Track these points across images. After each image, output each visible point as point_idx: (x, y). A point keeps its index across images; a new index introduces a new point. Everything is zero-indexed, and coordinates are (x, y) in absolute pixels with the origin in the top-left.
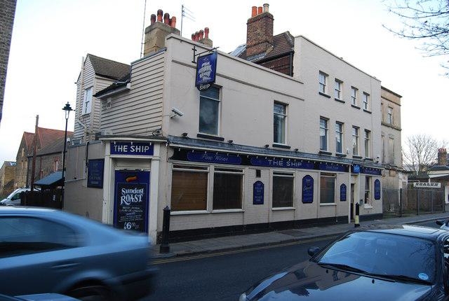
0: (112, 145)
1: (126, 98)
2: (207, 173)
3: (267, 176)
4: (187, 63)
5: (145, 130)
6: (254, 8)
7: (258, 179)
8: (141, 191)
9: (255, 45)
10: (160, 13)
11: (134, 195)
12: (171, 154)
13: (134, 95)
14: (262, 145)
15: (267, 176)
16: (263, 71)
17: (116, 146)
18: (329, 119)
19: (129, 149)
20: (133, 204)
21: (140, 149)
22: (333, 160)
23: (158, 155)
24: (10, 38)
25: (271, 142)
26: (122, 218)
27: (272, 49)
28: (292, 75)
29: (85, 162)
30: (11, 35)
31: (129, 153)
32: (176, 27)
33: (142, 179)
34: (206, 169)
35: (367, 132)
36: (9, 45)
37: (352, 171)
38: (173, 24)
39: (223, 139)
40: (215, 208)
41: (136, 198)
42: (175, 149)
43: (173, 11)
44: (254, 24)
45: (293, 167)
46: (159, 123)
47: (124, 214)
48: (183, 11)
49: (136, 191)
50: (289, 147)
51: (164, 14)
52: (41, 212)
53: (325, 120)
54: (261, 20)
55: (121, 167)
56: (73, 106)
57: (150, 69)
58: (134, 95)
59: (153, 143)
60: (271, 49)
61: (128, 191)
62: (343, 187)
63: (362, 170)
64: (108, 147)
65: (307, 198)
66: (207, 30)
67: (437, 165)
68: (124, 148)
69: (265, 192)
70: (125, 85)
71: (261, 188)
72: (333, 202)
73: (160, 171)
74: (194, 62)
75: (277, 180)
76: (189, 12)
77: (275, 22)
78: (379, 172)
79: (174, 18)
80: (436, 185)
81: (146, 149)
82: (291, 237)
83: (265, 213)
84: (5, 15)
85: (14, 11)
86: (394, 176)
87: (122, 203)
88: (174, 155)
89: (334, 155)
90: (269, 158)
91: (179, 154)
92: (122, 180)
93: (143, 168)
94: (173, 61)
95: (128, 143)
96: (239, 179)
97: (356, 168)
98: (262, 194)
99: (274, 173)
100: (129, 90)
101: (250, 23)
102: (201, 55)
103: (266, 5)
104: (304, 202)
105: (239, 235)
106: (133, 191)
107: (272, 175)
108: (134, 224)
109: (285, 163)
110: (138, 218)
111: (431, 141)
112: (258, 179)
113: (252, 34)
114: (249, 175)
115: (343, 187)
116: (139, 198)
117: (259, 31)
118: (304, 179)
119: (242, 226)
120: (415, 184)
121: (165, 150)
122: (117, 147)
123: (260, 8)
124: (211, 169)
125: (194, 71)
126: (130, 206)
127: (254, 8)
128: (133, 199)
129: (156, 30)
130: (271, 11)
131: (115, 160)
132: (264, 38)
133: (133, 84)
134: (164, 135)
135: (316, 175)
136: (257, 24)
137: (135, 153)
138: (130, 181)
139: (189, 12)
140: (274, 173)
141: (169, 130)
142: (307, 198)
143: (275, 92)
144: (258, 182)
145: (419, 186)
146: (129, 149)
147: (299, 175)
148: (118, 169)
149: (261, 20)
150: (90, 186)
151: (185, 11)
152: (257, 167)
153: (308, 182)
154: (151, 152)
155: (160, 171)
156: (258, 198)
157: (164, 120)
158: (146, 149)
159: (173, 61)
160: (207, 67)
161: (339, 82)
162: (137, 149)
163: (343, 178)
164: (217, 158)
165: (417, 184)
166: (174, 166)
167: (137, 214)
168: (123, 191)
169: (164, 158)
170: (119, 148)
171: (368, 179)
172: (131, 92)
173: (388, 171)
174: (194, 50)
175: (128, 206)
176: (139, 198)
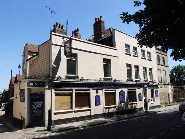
3: (102, 93)
7: (97, 94)
8: (41, 102)
10: (57, 24)
11: (38, 104)
14: (99, 79)
15: (102, 93)
20: (38, 108)
22: (134, 82)
25: (102, 76)
48: (67, 22)
51: (59, 24)
53: (129, 66)
56: (21, 66)
59: (45, 82)
63: (149, 86)
66: (78, 30)
69: (101, 99)
71: (99, 98)
75: (129, 92)
77: (105, 24)
78: (157, 86)
86: (167, 87)
89: (134, 80)
96: (88, 95)
98: (100, 100)
102: (66, 41)
104: (96, 105)
106: (37, 103)
109: (110, 85)
112: (97, 94)
114: (93, 93)
115: (140, 94)
116: (40, 106)
118: (120, 92)
122: (30, 84)
123: (98, 18)
126: (36, 109)
128: (38, 106)
135: (126, 91)
138: (36, 98)
153: (122, 94)
156: (98, 103)
160: (68, 45)
162: (38, 84)
167: (40, 113)
170: (30, 84)
173: (164, 85)
174: (63, 39)
176: (40, 106)
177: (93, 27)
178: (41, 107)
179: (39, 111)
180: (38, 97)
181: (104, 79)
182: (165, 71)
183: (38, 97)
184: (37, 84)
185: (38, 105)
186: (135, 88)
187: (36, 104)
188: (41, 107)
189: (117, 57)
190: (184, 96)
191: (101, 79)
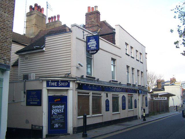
0: (48, 82)
1: (42, 55)
2: (89, 96)
3: (110, 95)
4: (80, 39)
5: (58, 73)
6: (89, 8)
8: (63, 106)
9: (91, 27)
11: (59, 109)
12: (77, 86)
13: (46, 55)
14: (108, 81)
16: (107, 43)
17: (50, 83)
18: (129, 67)
19: (58, 84)
21: (63, 84)
23: (72, 87)
24: (13, 24)
26: (53, 122)
27: (99, 32)
28: (115, 44)
29: (23, 92)
30: (13, 23)
31: (58, 86)
32: (44, 14)
33: (63, 100)
34: (89, 94)
35: (142, 72)
36: (12, 28)
37: (138, 93)
38: (42, 11)
39: (95, 78)
40: (93, 113)
41: (60, 110)
42: (79, 84)
43: (43, 5)
44: (90, 16)
45: (118, 91)
46: (69, 70)
47: (54, 119)
49: (60, 106)
50: (117, 82)
52: (96, 114)
54: (93, 15)
55: (51, 94)
57: (62, 41)
58: (46, 55)
59: (70, 81)
60: (99, 30)
61: (56, 107)
62: (135, 101)
64: (45, 84)
65: (124, 108)
66: (58, 16)
67: (156, 88)
68: (55, 84)
70: (43, 48)
72: (132, 109)
73: (72, 95)
74: (83, 38)
76: (50, 6)
79: (43, 9)
80: (165, 98)
81: (67, 84)
82: (123, 127)
83: (108, 116)
84: (10, 11)
85: (14, 10)
87: (52, 113)
88: (78, 86)
90: (111, 87)
91: (81, 86)
92: (51, 100)
93: (64, 94)
94: (77, 38)
95: (57, 81)
97: (140, 91)
99: (112, 95)
100: (44, 51)
101: (87, 15)
103: (96, 7)
105: (111, 125)
106: (58, 107)
107: (112, 96)
108: (60, 124)
110: (62, 121)
111: (154, 76)
113: (89, 21)
115: (107, 101)
117: (93, 20)
119: (103, 122)
120: (154, 98)
121: (74, 84)
122: (51, 83)
123: (93, 8)
124: (91, 93)
125: (84, 44)
127: (89, 8)
129: (35, 15)
130: (99, 9)
131: (48, 90)
132: (96, 24)
133: (46, 48)
134: (72, 76)
136: (91, 16)
137: (61, 86)
138: (57, 101)
139: (50, 6)
140: (112, 95)
141: (75, 74)
142: (124, 108)
143: (112, 53)
144: (107, 99)
145: (156, 99)
146: (58, 84)
147: (121, 95)
148: (50, 95)
149: (93, 15)
150: (28, 104)
151: (49, 5)
152: (107, 92)
154: (68, 86)
155: (72, 95)
157: (72, 68)
158: (67, 84)
159: (77, 38)
161: (132, 48)
163: (135, 96)
164: (93, 88)
165: (155, 99)
166: (78, 93)
167: (61, 119)
168: (53, 107)
169: (74, 89)
171: (143, 96)
172: (45, 53)
175: (56, 115)
176: (62, 111)
177: (85, 17)
178: (63, 112)
179: (61, 116)
180: (59, 99)
181: (87, 77)
182: (137, 60)
183: (59, 99)
184: (61, 84)
185: (59, 110)
186: (148, 106)
187: (56, 108)
188: (63, 112)
189: (121, 57)
190: (1, 59)
191: (83, 76)
